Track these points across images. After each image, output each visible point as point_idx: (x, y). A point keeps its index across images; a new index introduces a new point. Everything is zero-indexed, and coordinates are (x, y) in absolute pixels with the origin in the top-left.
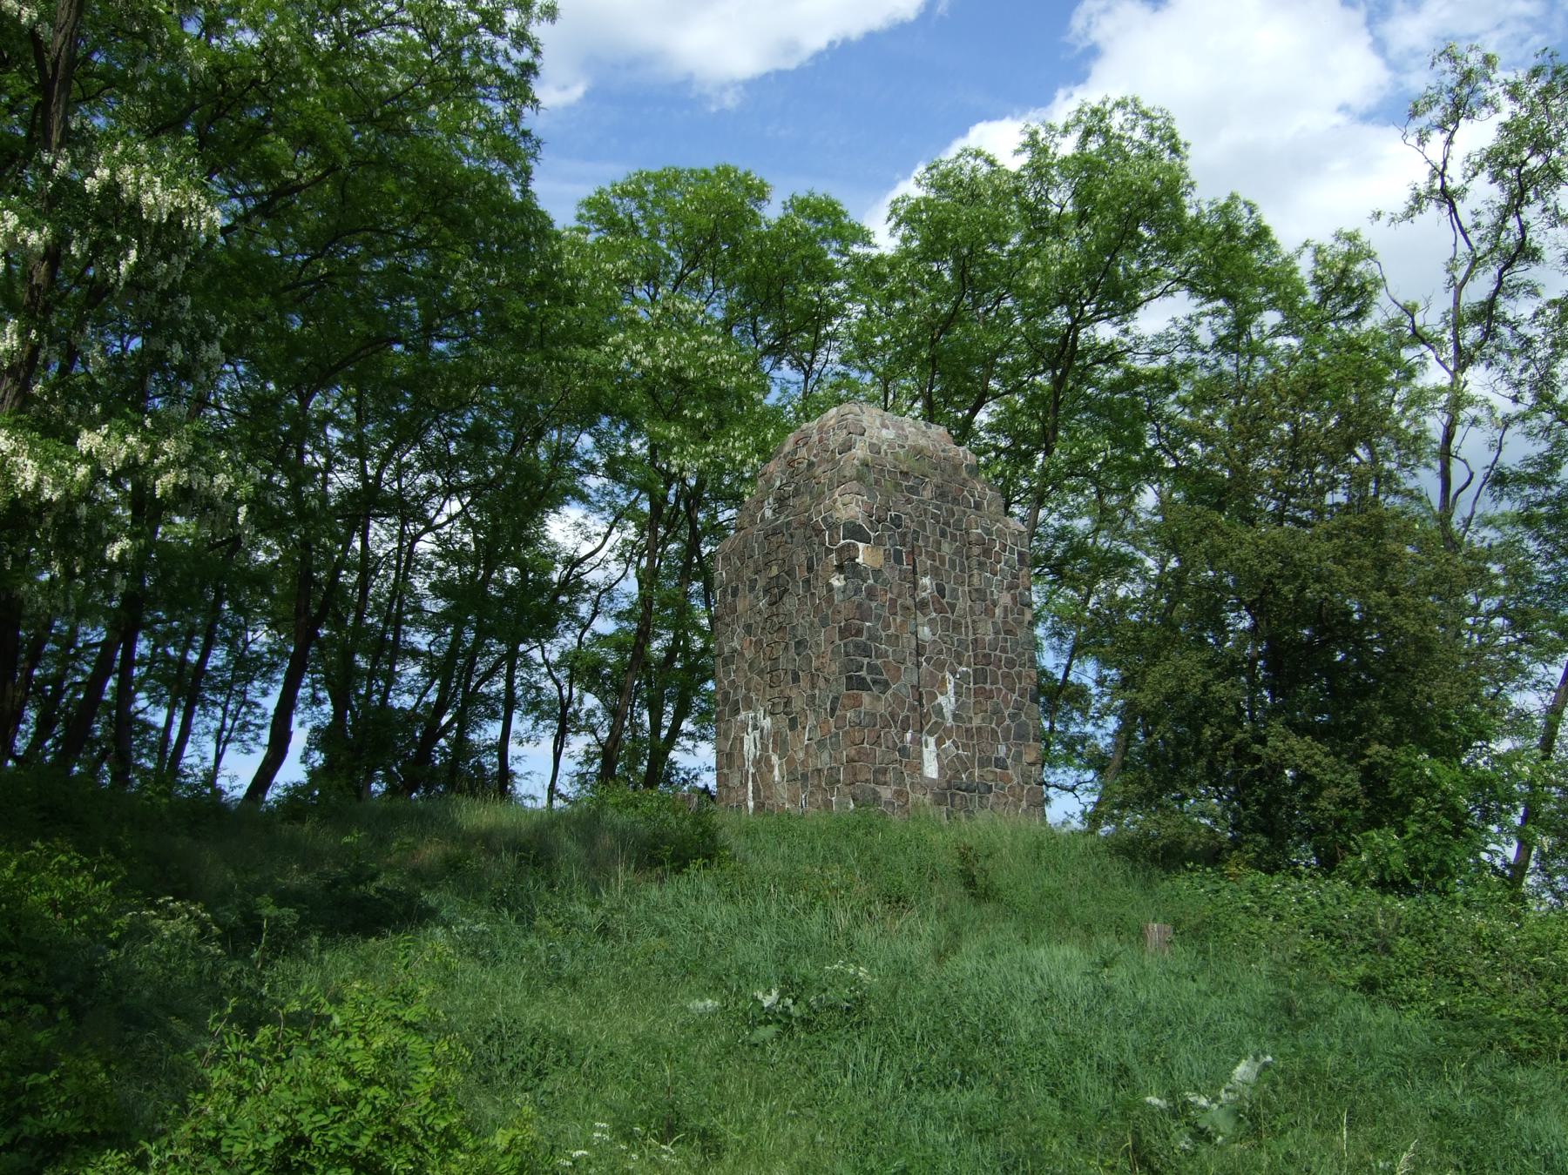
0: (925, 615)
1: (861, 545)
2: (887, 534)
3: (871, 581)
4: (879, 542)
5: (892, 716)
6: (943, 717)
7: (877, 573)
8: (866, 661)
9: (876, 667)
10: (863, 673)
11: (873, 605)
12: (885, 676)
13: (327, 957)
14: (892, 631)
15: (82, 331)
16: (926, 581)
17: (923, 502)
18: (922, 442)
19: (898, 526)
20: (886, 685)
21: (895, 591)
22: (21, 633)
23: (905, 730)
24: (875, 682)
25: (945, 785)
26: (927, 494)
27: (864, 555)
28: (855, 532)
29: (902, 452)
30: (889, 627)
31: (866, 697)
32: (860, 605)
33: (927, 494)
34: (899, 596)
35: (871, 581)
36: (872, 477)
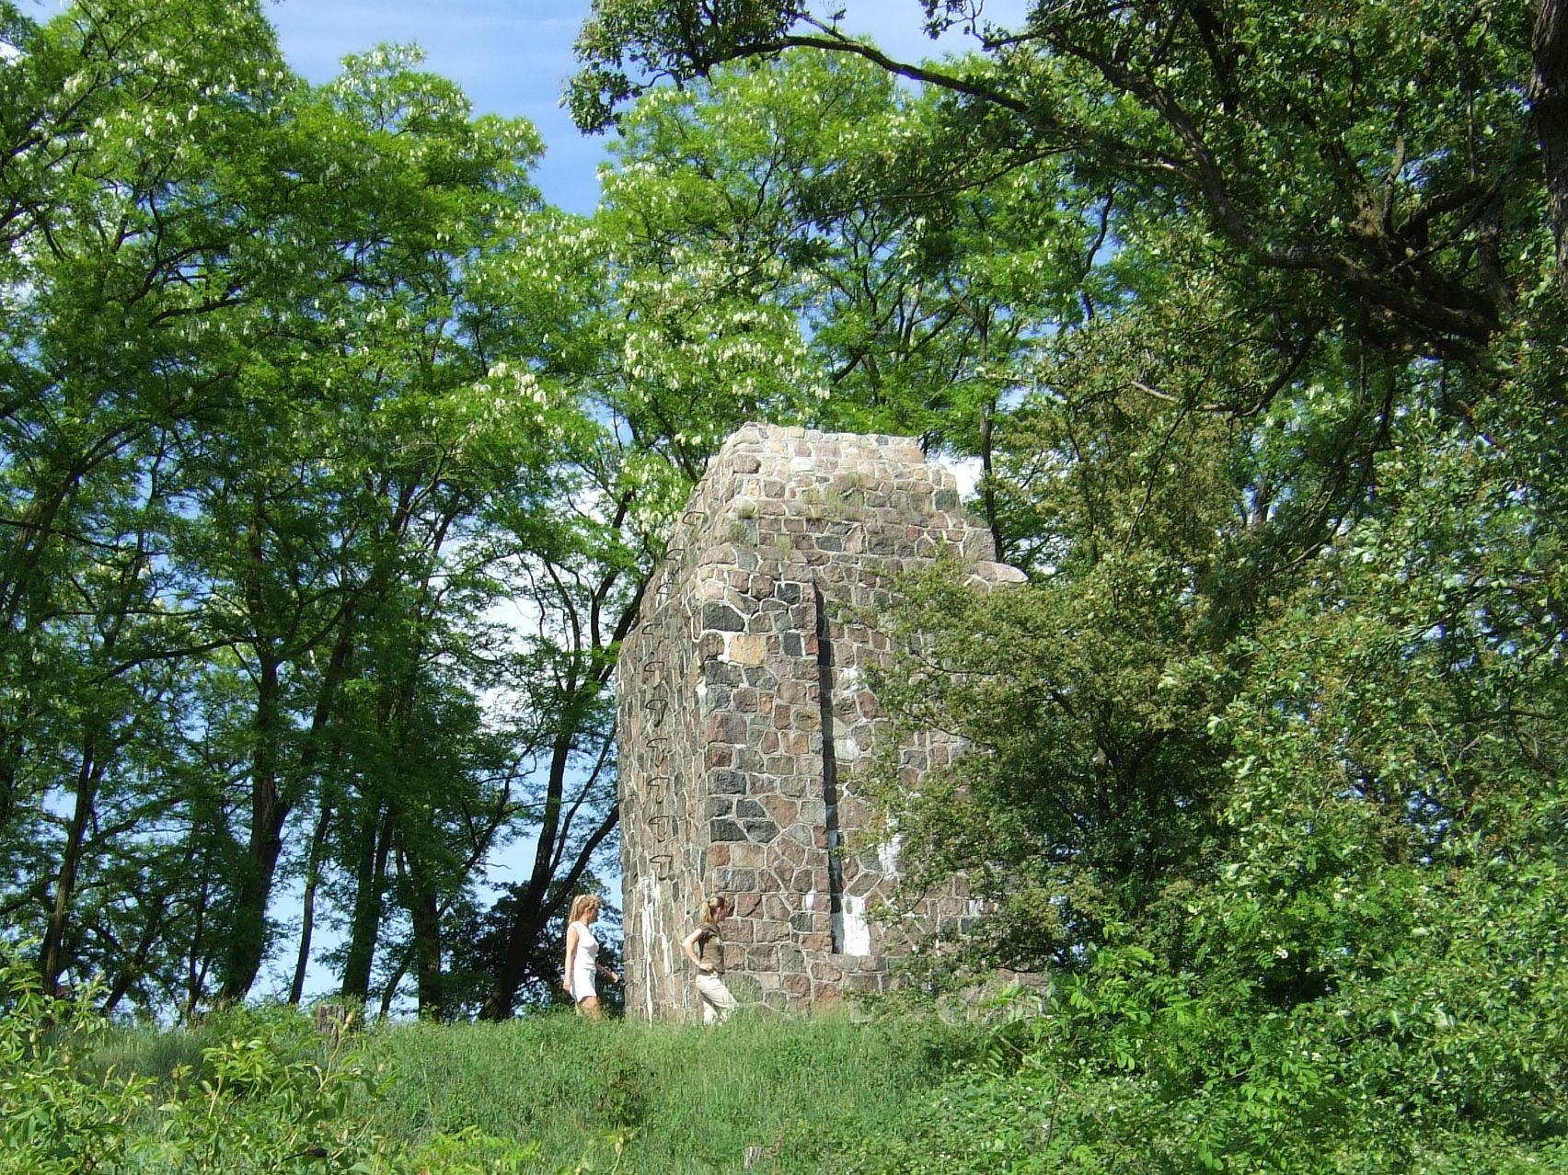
0: (848, 723)
1: (727, 636)
2: (771, 614)
3: (744, 685)
4: (758, 626)
5: (781, 873)
6: (879, 867)
7: (754, 672)
8: (735, 798)
9: (754, 805)
10: (731, 817)
11: (748, 718)
12: (769, 818)
13: (1348, 849)
14: (781, 751)
15: (1041, 244)
16: (851, 673)
17: (846, 559)
18: (863, 468)
19: (792, 601)
20: (771, 828)
21: (786, 695)
22: (254, 708)
23: (802, 892)
24: (750, 828)
25: (873, 965)
26: (854, 546)
27: (734, 649)
28: (720, 618)
29: (821, 487)
30: (775, 746)
31: (736, 850)
32: (725, 722)
33: (854, 546)
34: (793, 700)
35: (744, 685)
36: (754, 536)
